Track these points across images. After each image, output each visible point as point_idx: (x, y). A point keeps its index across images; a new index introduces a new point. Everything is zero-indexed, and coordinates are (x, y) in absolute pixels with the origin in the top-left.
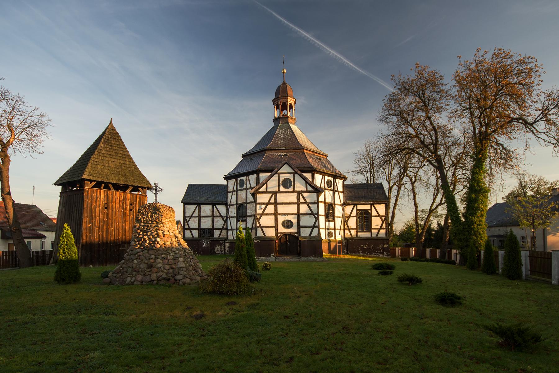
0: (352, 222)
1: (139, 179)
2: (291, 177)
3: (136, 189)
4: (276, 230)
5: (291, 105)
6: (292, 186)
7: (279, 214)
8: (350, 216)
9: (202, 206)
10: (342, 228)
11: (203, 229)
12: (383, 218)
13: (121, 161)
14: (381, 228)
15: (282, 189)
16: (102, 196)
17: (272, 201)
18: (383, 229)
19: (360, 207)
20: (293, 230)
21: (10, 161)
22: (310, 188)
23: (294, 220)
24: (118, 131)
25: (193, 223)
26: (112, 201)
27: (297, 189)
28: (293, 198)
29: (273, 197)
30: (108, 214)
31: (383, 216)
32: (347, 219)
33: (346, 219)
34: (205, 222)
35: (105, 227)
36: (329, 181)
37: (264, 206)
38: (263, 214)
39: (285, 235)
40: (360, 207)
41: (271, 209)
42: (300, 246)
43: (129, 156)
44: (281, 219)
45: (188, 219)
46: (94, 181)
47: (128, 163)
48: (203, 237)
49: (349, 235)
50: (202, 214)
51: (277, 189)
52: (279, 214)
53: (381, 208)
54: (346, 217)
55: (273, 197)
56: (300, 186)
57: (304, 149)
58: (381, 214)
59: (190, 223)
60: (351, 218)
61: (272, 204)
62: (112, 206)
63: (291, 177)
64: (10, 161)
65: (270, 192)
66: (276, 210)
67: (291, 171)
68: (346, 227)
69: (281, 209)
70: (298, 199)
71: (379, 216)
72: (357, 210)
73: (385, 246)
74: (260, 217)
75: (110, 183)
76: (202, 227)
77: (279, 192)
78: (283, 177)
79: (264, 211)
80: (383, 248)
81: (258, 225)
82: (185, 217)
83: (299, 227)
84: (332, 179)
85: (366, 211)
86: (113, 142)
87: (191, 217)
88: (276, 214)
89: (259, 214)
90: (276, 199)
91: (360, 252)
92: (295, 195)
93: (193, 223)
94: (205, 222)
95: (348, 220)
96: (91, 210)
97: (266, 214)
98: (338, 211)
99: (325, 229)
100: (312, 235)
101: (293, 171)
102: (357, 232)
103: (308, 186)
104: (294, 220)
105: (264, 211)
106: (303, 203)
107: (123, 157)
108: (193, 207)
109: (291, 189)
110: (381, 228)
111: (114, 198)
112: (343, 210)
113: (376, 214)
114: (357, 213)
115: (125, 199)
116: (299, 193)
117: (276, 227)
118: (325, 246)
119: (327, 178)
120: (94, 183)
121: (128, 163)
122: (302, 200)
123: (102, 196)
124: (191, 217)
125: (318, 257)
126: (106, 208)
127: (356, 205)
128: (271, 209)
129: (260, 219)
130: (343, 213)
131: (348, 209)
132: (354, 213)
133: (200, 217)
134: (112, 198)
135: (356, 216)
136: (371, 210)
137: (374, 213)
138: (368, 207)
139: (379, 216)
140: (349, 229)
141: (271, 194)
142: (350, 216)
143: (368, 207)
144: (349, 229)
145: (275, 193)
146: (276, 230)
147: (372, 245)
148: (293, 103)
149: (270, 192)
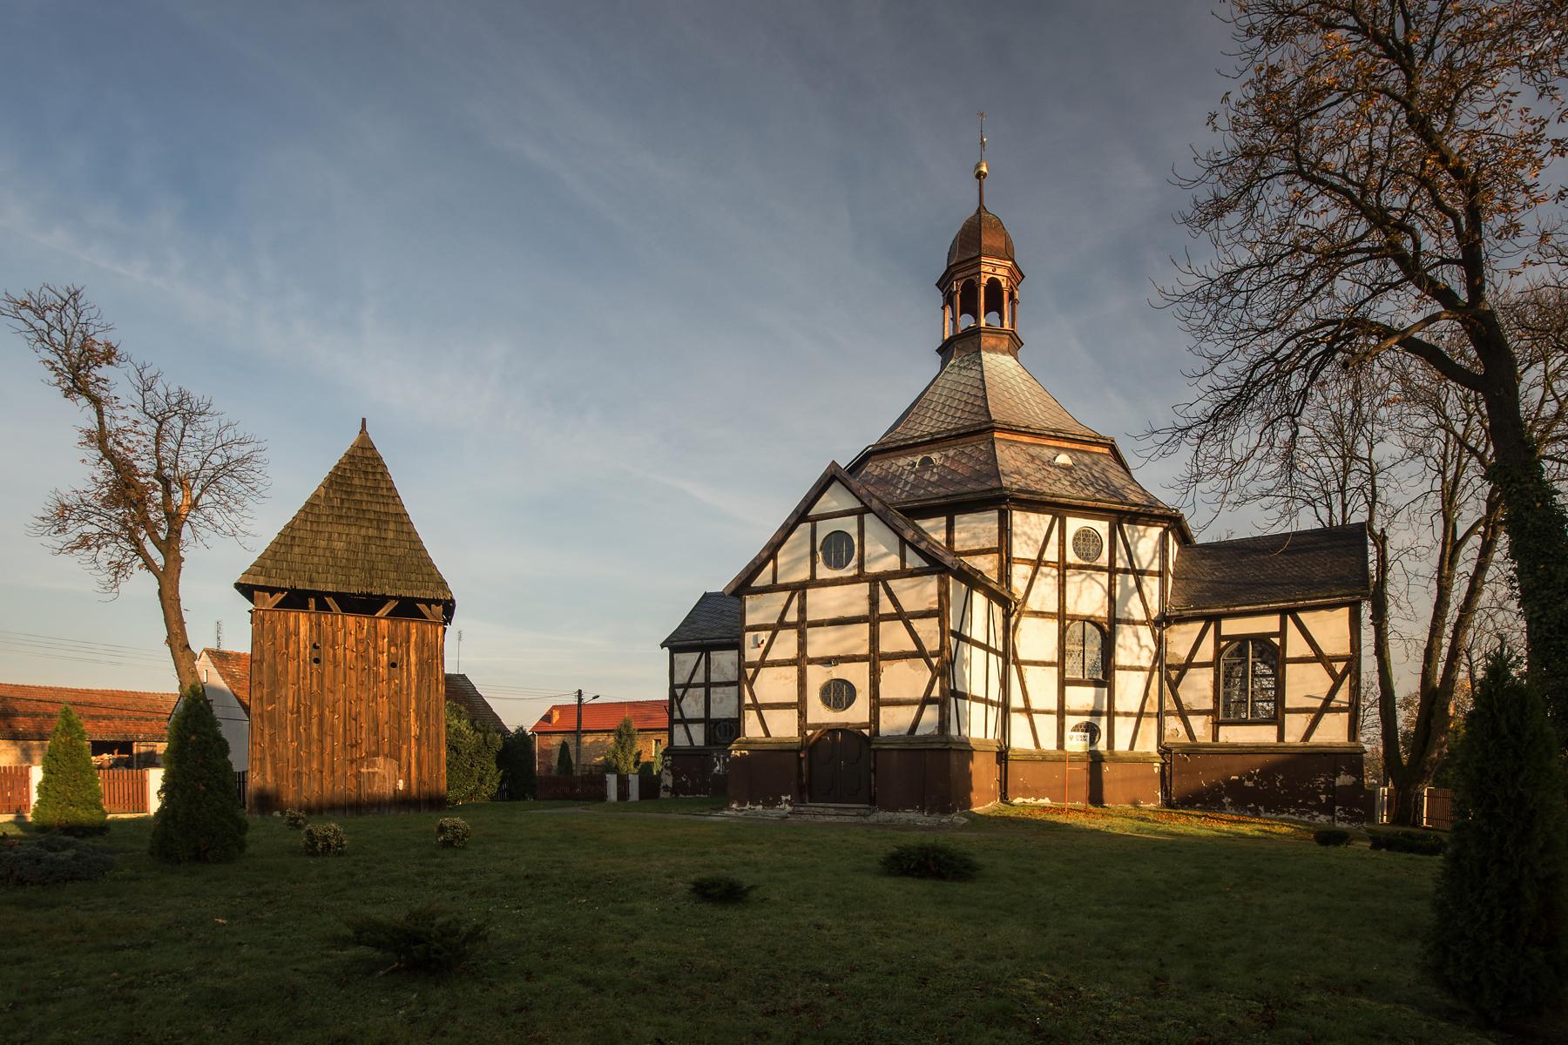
0: (1199, 687)
1: (413, 577)
2: (849, 525)
3: (407, 609)
4: (802, 715)
5: (994, 285)
6: (854, 562)
7: (812, 661)
8: (1189, 663)
9: (713, 654)
10: (1152, 707)
11: (718, 721)
12: (1339, 667)
13: (371, 532)
14: (1326, 707)
15: (824, 573)
16: (304, 629)
17: (792, 617)
18: (1338, 710)
19: (1231, 627)
20: (857, 713)
21: (182, 560)
22: (914, 561)
23: (857, 674)
24: (381, 450)
25: (692, 706)
26: (334, 643)
27: (873, 568)
28: (853, 599)
29: (795, 603)
30: (321, 676)
31: (1338, 659)
32: (1174, 674)
33: (1169, 673)
34: (722, 700)
35: (315, 712)
36: (1085, 536)
37: (764, 636)
38: (763, 663)
39: (832, 730)
40: (1231, 627)
41: (786, 646)
42: (874, 770)
43: (402, 518)
44: (817, 677)
45: (679, 692)
46: (282, 590)
47: (391, 535)
48: (716, 744)
49: (1183, 738)
50: (714, 678)
51: (803, 574)
52: (812, 661)
53: (1330, 629)
54: (1169, 667)
55: (795, 603)
56: (882, 554)
57: (993, 429)
58: (1328, 649)
59: (684, 703)
60: (1191, 671)
61: (789, 626)
62: (335, 656)
63: (849, 525)
64: (182, 560)
65: (785, 588)
66: (802, 646)
67: (854, 504)
68: (1169, 704)
69: (821, 642)
70: (874, 601)
71: (1319, 657)
72: (1218, 637)
73: (1343, 780)
74: (756, 673)
75: (329, 594)
76: (714, 714)
77: (813, 582)
78: (825, 529)
79: (766, 652)
80: (1330, 788)
81: (748, 700)
82: (673, 687)
83: (877, 703)
84: (1102, 527)
85: (1261, 640)
86: (356, 481)
87: (687, 686)
88: (801, 661)
89: (751, 665)
90: (802, 610)
91: (1227, 800)
92: (864, 588)
93: (692, 706)
94: (722, 700)
95: (1180, 678)
96: (273, 667)
97: (774, 664)
98: (1134, 647)
99: (1111, 714)
100: (918, 733)
101: (856, 505)
102: (1217, 724)
103: (909, 553)
104: (857, 674)
105: (766, 652)
106: (889, 617)
107: (379, 520)
108: (692, 658)
109: (850, 570)
110: (1326, 707)
111: (340, 635)
112: (1159, 641)
113: (1307, 651)
114: (1218, 652)
115: (375, 634)
116: (878, 580)
117: (801, 706)
118: (983, 772)
119: (1074, 524)
120: (279, 597)
121: (391, 535)
122: (886, 606)
123: (304, 629)
124: (687, 686)
125: (931, 812)
126: (317, 661)
127: (1216, 619)
128: (786, 646)
129: (753, 679)
130: (1159, 656)
131: (1181, 640)
132: (1207, 651)
133: (708, 685)
134: (334, 634)
135: (1214, 664)
136: (1282, 634)
137: (1296, 645)
138: (1270, 624)
139: (1319, 657)
140: (1183, 713)
141: (1201, 625)
142: (1189, 663)
143: (1270, 624)
144: (1183, 713)
145: (799, 589)
146: (802, 715)
147: (1293, 779)
148: (1002, 275)
149: (785, 588)
